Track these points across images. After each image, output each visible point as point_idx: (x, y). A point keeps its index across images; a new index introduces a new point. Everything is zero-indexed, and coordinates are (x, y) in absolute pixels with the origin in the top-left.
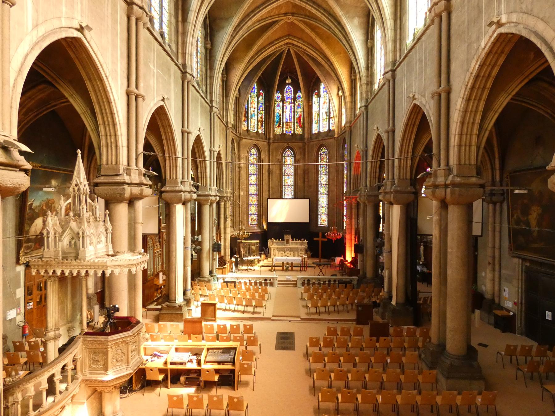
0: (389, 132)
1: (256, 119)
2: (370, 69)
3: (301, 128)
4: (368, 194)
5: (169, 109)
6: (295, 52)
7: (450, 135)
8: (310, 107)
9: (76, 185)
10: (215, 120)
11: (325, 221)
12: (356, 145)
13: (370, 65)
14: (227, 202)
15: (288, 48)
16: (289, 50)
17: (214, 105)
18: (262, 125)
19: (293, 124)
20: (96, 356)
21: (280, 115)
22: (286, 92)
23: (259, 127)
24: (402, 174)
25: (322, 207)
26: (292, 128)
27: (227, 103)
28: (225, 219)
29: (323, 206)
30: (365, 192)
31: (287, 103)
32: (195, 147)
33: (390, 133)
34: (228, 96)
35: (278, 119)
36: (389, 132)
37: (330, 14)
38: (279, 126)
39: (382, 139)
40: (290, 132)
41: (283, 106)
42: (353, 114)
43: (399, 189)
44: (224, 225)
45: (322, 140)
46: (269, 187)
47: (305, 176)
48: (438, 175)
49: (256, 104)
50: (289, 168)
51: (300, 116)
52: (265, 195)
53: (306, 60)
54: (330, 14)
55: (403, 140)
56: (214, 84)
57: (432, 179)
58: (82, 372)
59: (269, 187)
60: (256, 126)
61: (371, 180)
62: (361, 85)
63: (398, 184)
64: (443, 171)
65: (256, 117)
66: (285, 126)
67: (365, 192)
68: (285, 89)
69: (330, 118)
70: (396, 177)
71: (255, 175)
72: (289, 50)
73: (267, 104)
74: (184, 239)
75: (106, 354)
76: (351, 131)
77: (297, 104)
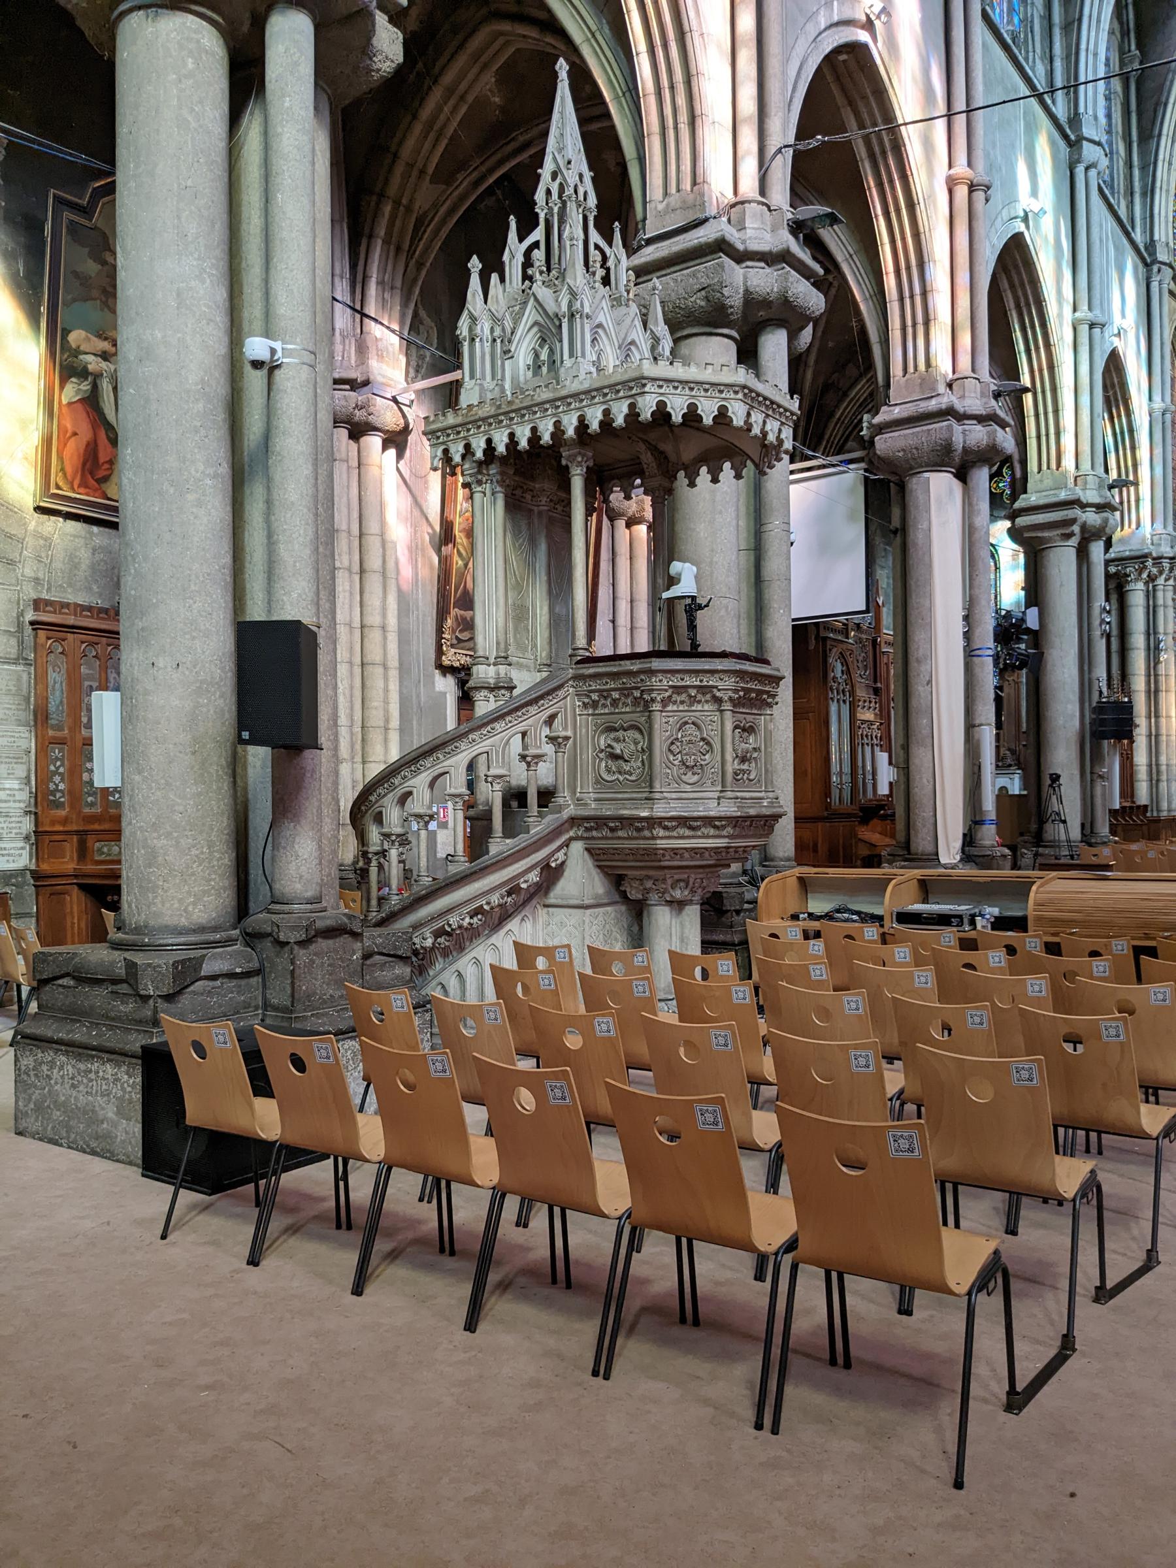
5: (892, 72)
9: (554, 176)
10: (1095, 218)
14: (1161, 581)
17: (1088, 131)
20: (617, 740)
32: (1005, 284)
34: (1151, 137)
44: (1148, 683)
56: (1083, 46)
58: (574, 792)
74: (966, 618)
75: (647, 731)
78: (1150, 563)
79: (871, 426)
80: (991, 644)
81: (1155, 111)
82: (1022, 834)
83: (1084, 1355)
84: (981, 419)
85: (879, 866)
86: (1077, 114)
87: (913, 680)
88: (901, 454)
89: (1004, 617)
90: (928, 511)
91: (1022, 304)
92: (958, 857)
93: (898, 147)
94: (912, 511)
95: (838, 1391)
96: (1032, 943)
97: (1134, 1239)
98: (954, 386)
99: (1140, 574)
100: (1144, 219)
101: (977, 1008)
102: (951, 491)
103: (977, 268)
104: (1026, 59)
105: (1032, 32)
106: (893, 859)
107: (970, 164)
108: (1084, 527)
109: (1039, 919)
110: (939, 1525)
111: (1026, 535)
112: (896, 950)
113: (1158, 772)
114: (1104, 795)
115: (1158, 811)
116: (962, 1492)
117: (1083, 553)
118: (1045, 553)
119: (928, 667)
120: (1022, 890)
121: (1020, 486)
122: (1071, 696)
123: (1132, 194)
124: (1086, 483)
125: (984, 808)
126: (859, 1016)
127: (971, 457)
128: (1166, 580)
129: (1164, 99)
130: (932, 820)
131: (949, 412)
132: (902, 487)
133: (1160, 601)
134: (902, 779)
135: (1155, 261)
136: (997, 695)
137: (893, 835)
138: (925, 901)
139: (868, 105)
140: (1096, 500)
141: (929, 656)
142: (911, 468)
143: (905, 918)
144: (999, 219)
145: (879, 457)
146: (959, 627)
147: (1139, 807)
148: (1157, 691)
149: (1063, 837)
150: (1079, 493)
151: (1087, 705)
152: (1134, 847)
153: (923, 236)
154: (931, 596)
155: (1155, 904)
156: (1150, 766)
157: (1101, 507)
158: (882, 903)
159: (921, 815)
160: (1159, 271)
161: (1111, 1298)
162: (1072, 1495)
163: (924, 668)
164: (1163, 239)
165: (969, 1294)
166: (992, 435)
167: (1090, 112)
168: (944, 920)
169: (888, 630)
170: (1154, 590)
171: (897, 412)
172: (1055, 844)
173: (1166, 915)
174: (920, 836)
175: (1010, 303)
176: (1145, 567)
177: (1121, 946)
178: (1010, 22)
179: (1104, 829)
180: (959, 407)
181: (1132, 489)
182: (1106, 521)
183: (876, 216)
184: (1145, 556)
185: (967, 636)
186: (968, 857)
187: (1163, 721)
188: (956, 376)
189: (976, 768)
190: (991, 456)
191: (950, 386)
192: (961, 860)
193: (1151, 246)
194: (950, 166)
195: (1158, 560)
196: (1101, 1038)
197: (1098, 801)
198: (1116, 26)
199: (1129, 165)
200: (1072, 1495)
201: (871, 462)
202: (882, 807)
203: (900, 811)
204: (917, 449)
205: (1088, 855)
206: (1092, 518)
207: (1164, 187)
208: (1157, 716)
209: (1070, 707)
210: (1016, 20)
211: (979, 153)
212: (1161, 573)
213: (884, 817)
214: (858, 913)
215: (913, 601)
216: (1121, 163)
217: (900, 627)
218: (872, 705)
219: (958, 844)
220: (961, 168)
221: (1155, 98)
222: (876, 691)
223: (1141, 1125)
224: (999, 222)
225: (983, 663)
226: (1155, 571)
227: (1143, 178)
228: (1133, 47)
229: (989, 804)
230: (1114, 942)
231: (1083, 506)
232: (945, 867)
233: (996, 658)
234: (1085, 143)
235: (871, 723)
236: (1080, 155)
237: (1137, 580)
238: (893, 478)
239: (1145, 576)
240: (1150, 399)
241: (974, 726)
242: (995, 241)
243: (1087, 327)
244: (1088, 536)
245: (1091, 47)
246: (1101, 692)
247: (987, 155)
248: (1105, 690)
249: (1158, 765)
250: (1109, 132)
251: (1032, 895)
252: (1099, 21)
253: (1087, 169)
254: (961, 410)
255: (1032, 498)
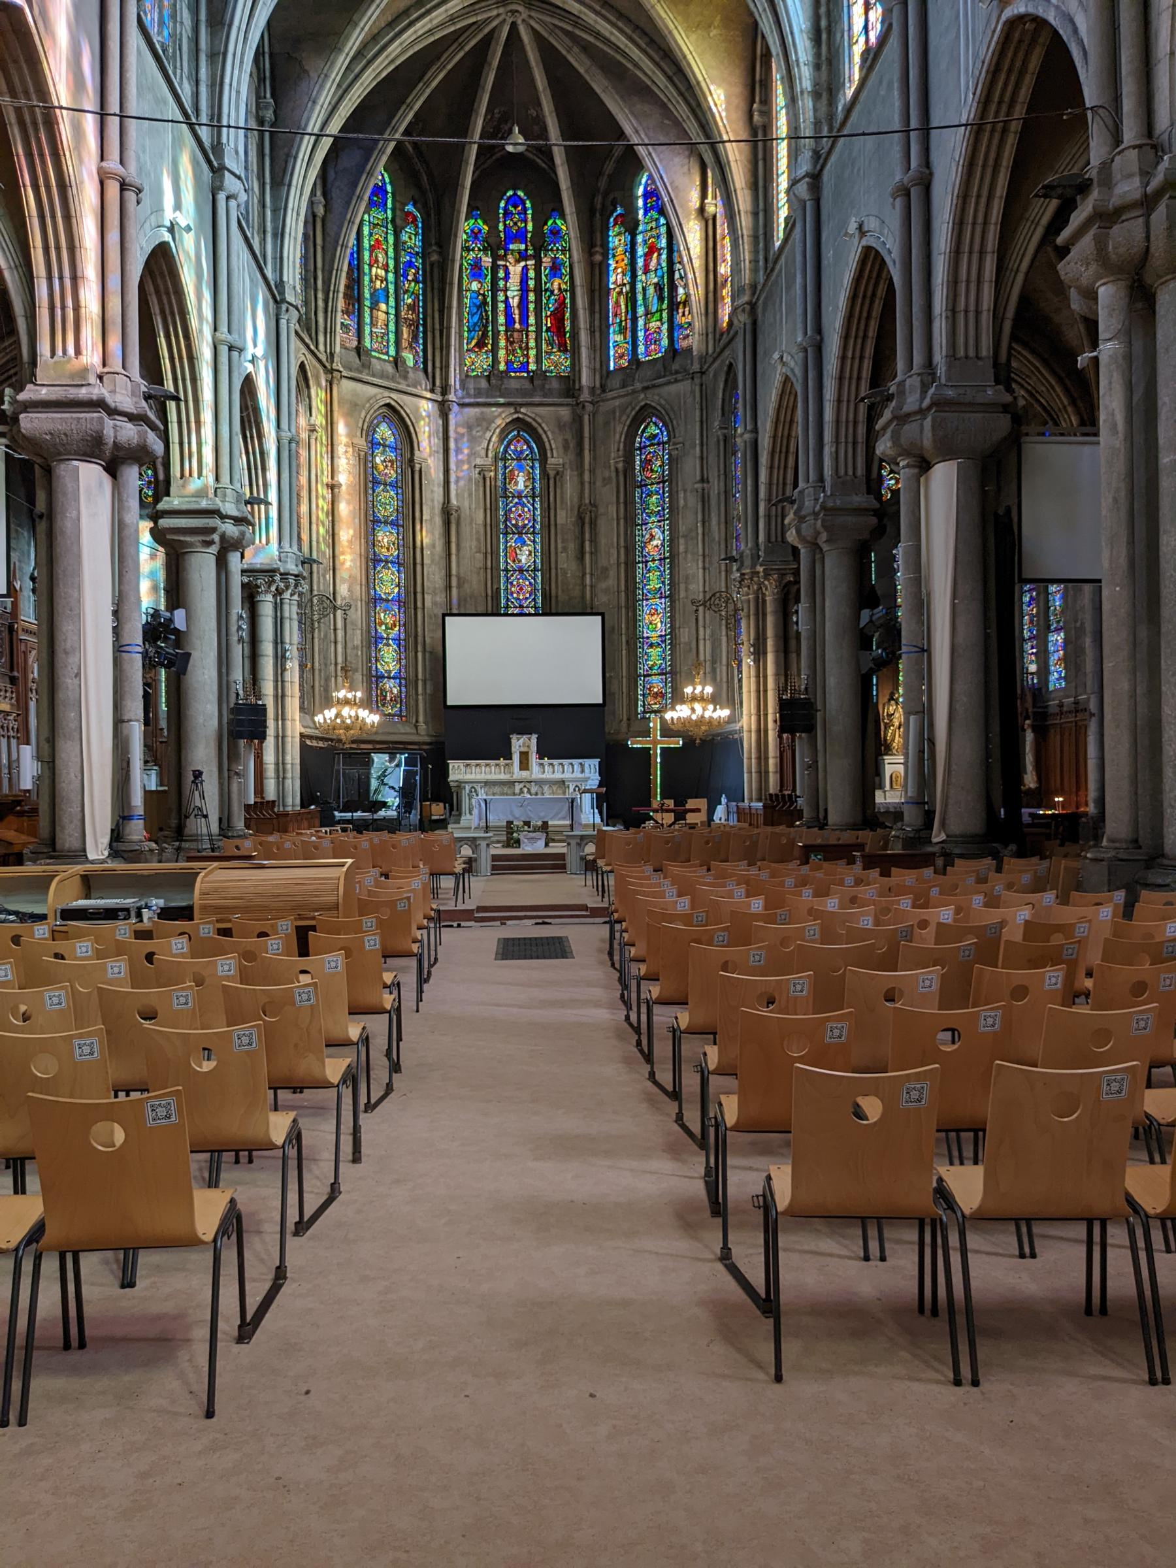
0: (907, 194)
1: (392, 311)
2: (824, 36)
3: (565, 351)
4: (830, 504)
6: (536, 35)
7: (1153, 14)
8: (597, 272)
11: (663, 695)
12: (776, 356)
13: (823, 23)
14: (287, 595)
15: (509, 21)
16: (514, 25)
18: (415, 338)
19: (532, 335)
21: (485, 303)
22: (507, 213)
23: (405, 344)
24: (961, 340)
25: (651, 645)
26: (532, 353)
27: (280, 210)
28: (280, 659)
29: (654, 640)
30: (817, 500)
31: (510, 258)
32: (150, 288)
33: (914, 192)
34: (282, 183)
35: (476, 318)
36: (907, 194)
37: (652, 42)
38: (481, 344)
39: (883, 261)
40: (524, 366)
41: (495, 268)
42: (761, 257)
43: (950, 393)
45: (646, 388)
46: (449, 575)
47: (582, 533)
48: (1117, 176)
49: (391, 253)
50: (524, 505)
51: (562, 304)
52: (433, 601)
53: (582, 71)
54: (652, 42)
55: (964, 196)
56: (227, 80)
57: (1095, 194)
59: (449, 575)
60: (392, 337)
61: (837, 452)
62: (792, 100)
63: (948, 379)
64: (1133, 154)
65: (392, 302)
66: (502, 343)
67: (817, 500)
68: (502, 204)
69: (673, 307)
70: (939, 357)
71: (392, 523)
72: (514, 25)
73: (435, 257)
74: (115, 613)
76: (755, 323)
77: (546, 261)
78: (278, 578)
79: (14, 401)
80: (140, 641)
81: (286, 162)
82: (161, 829)
83: (294, 1281)
84: (132, 418)
85: (20, 863)
86: (219, 142)
87: (60, 672)
88: (48, 437)
89: (152, 616)
90: (77, 500)
91: (167, 312)
92: (106, 853)
93: (51, 124)
94: (59, 498)
95: (75, 1371)
96: (205, 928)
97: (317, 1178)
98: (105, 379)
99: (269, 587)
100: (274, 258)
101: (183, 989)
102: (101, 484)
103: (128, 267)
104: (175, 74)
105: (180, 49)
106: (36, 857)
107: (121, 162)
108: (223, 537)
109: (204, 908)
110: (200, 1452)
111: (168, 537)
112: (78, 945)
113: (284, 770)
114: (240, 790)
115: (284, 806)
116: (213, 1420)
117: (222, 562)
118: (186, 557)
119: (77, 660)
120: (187, 881)
121: (162, 488)
122: (211, 697)
123: (264, 232)
124: (225, 495)
125: (133, 804)
126: (61, 1010)
127: (121, 454)
128: (292, 595)
129: (294, 153)
130: (79, 817)
131: (99, 404)
132: (48, 471)
133: (287, 614)
134: (47, 773)
135: (284, 300)
136: (145, 691)
137: (33, 832)
138: (88, 897)
139: (20, 70)
140: (235, 513)
141: (78, 648)
142: (60, 454)
143: (68, 914)
144: (148, 223)
145: (23, 435)
146: (108, 622)
147: (268, 802)
148: (283, 696)
149: (205, 831)
150: (218, 503)
151: (225, 706)
152: (271, 839)
153: (74, 220)
154: (80, 588)
155: (305, 887)
156: (277, 764)
157: (239, 521)
158: (45, 901)
159: (68, 812)
160: (287, 310)
161: (308, 1229)
162: (307, 1392)
163: (72, 660)
164: (291, 282)
165: (215, 1240)
166: (142, 435)
167: (232, 145)
168: (111, 914)
169: (28, 614)
170: (282, 603)
171: (44, 393)
172: (196, 839)
173: (316, 896)
174: (66, 832)
175: (155, 309)
176: (274, 581)
177: (286, 926)
178: (160, 33)
179: (239, 823)
180: (110, 400)
181: (262, 507)
182: (243, 534)
183: (24, 186)
184: (274, 571)
185: (116, 631)
186: (116, 852)
187: (289, 723)
188: (106, 370)
189: (125, 765)
190: (140, 455)
191: (101, 378)
192: (110, 855)
193: (280, 284)
194: (102, 159)
195: (285, 575)
196: (294, 1004)
197: (235, 796)
198: (255, 71)
199: (263, 205)
200: (307, 1392)
201: (13, 439)
202: (19, 803)
203: (44, 807)
204: (66, 435)
205: (229, 847)
206: (230, 529)
207: (293, 234)
208: (283, 719)
209: (209, 706)
210: (166, 33)
211: (131, 154)
212: (287, 587)
213: (21, 814)
214: (16, 913)
215: (61, 590)
216: (256, 201)
217: (45, 616)
218: (8, 694)
219: (106, 840)
220: (113, 164)
221: (286, 150)
222: (13, 681)
223: (325, 1076)
224: (147, 226)
225: (131, 659)
226: (282, 585)
227: (275, 219)
228: (268, 95)
229: (137, 800)
230: (280, 922)
231: (223, 517)
232: (92, 862)
233: (145, 655)
234: (226, 173)
235: (7, 714)
236: (222, 182)
237: (266, 592)
238: (39, 461)
239: (273, 589)
240: (278, 426)
241: (123, 721)
242: (144, 244)
243: (226, 348)
244: (229, 546)
245: (235, 84)
246: (238, 694)
247: (138, 158)
248: (241, 692)
249: (283, 764)
250: (246, 168)
251: (198, 885)
252: (242, 62)
253: (228, 198)
254: (113, 405)
255: (173, 502)
